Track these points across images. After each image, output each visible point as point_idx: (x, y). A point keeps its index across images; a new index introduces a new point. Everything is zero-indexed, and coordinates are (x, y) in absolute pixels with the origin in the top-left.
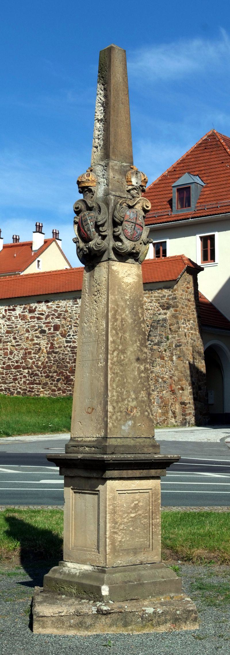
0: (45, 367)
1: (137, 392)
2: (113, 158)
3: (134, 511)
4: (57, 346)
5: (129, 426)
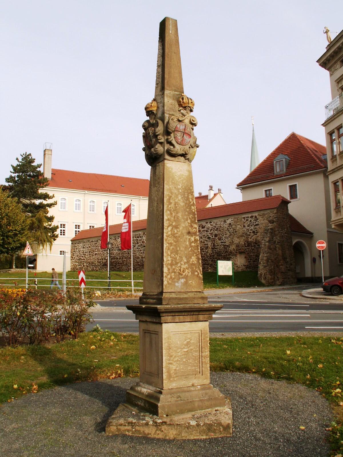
0: (211, 256)
3: (187, 347)
4: (216, 245)
5: (182, 283)
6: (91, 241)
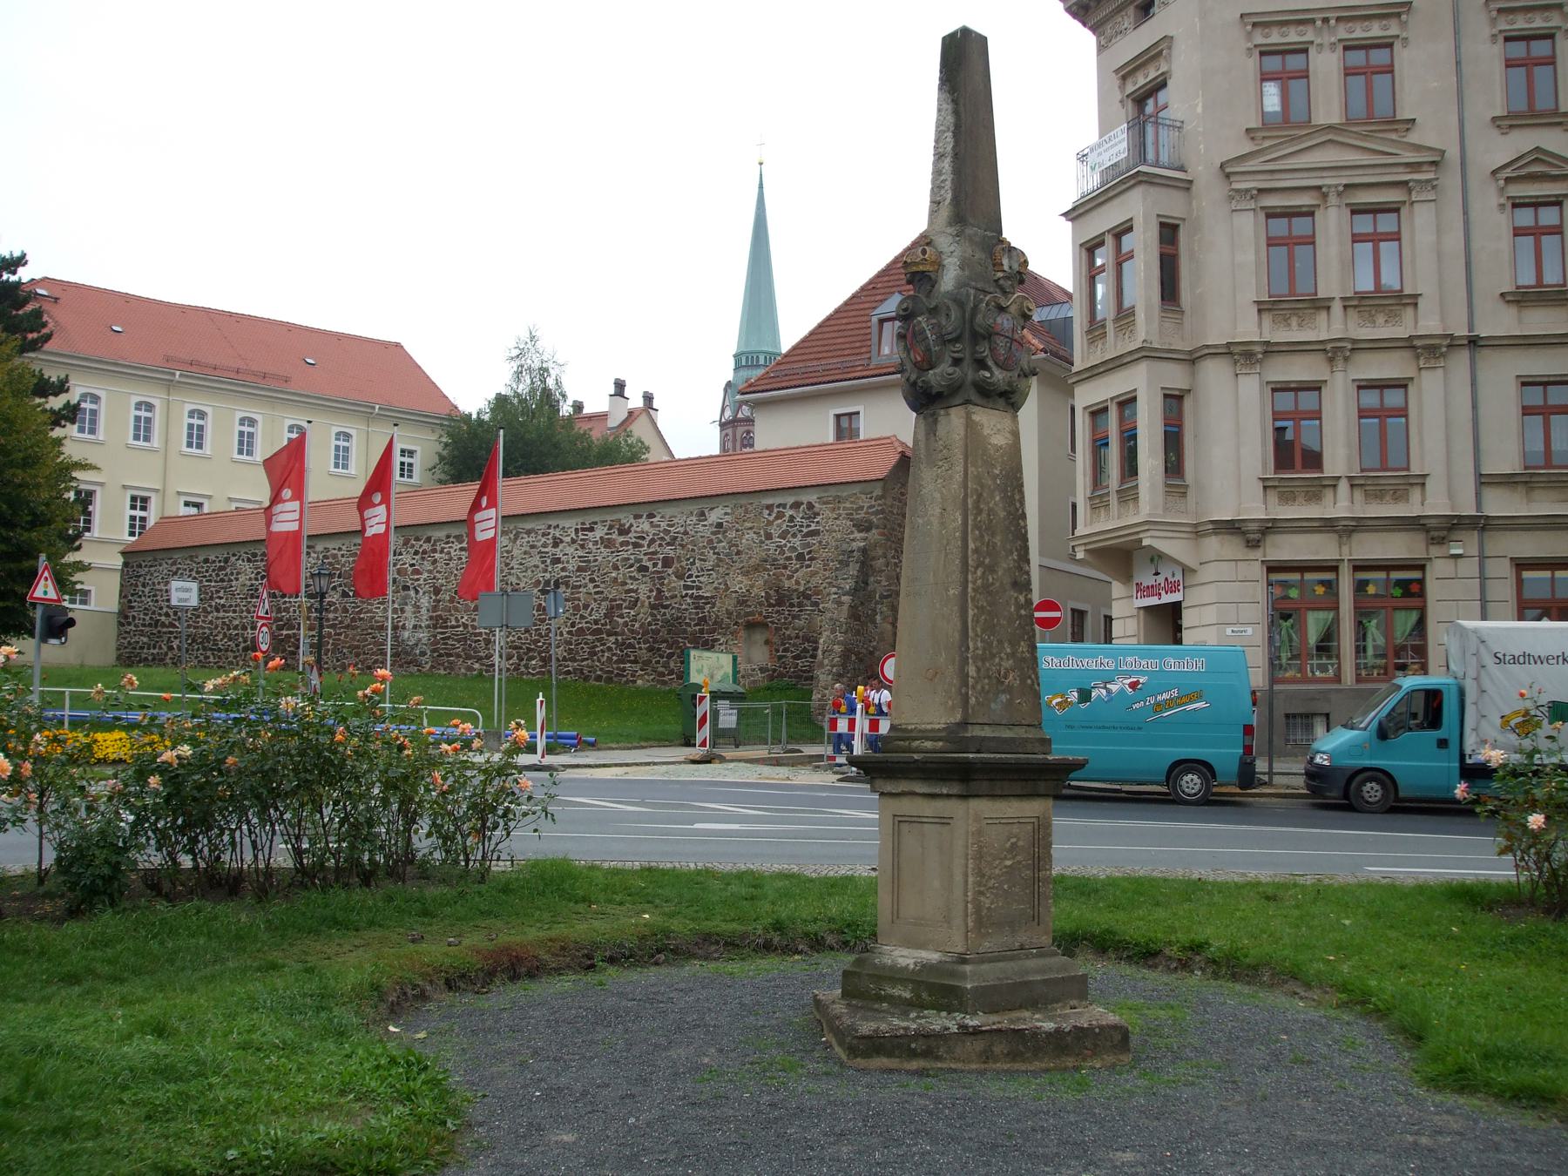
1: (1014, 644)
2: (971, 220)
6: (201, 558)
